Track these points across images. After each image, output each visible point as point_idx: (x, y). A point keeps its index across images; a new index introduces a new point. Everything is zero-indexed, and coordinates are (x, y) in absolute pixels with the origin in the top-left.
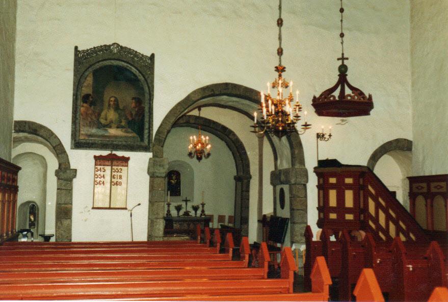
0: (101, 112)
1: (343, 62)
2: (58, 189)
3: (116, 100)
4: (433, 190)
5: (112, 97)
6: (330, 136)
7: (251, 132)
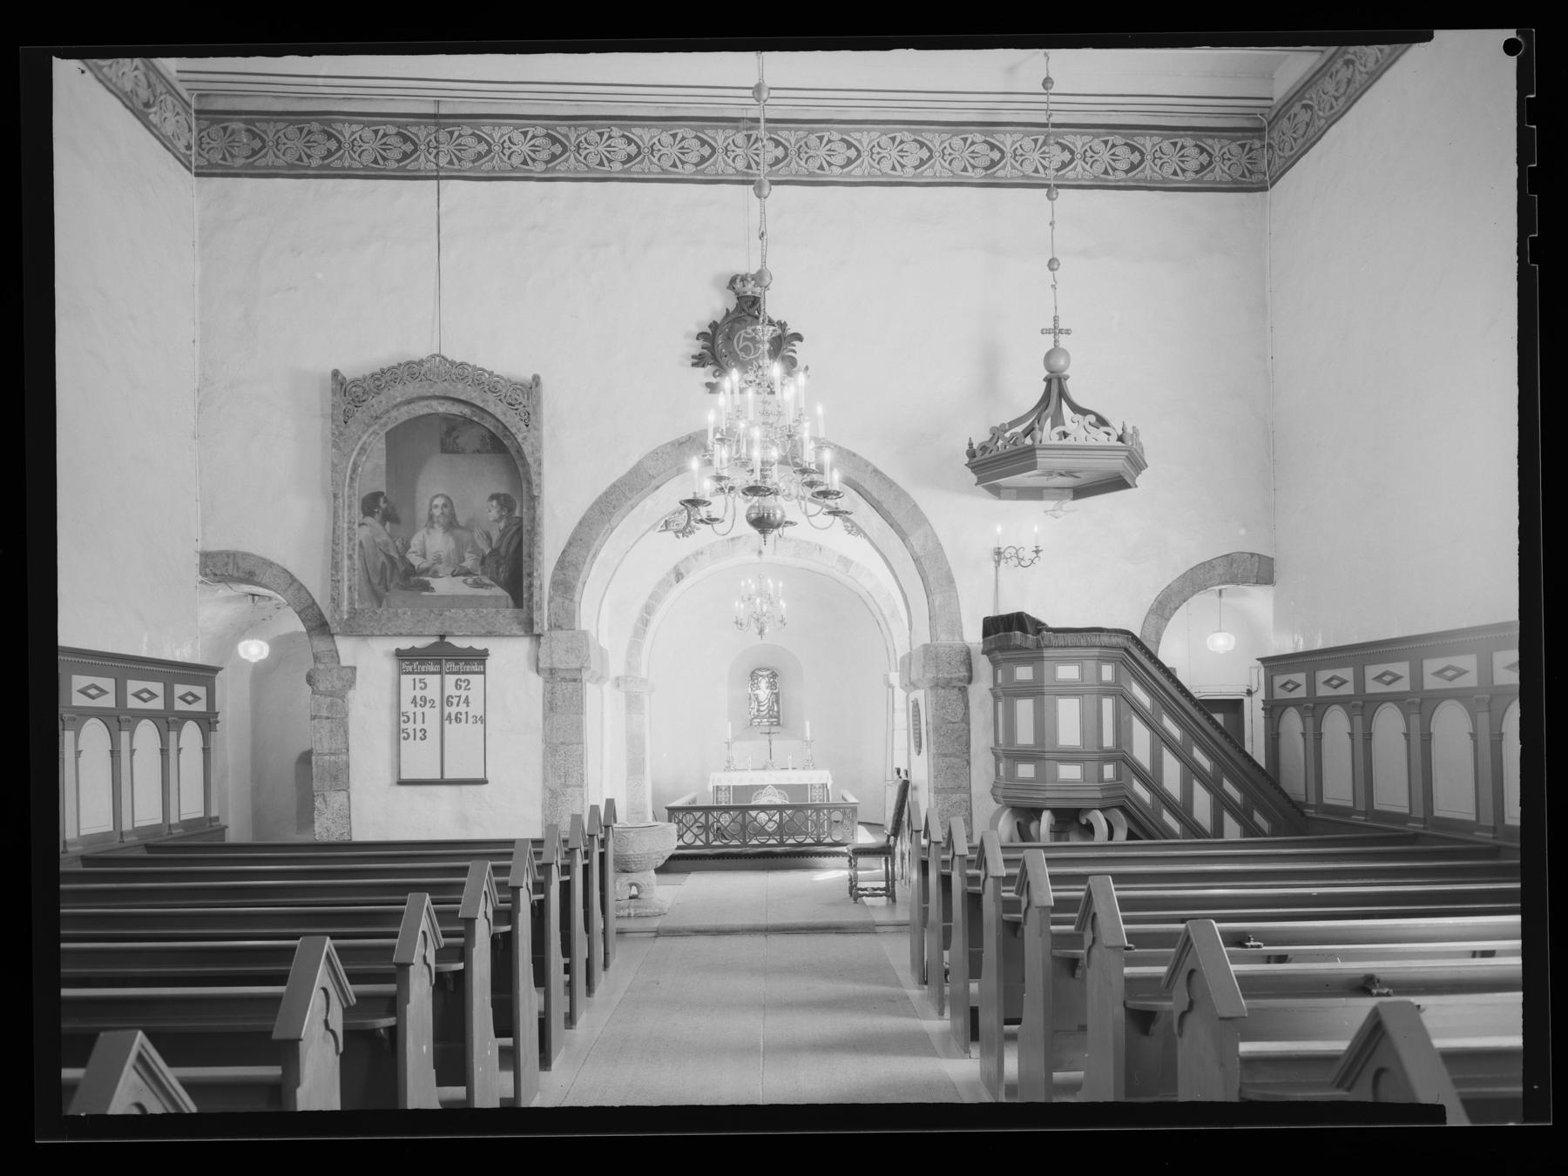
0: (411, 538)
3: (449, 503)
4: (1373, 688)
5: (437, 496)
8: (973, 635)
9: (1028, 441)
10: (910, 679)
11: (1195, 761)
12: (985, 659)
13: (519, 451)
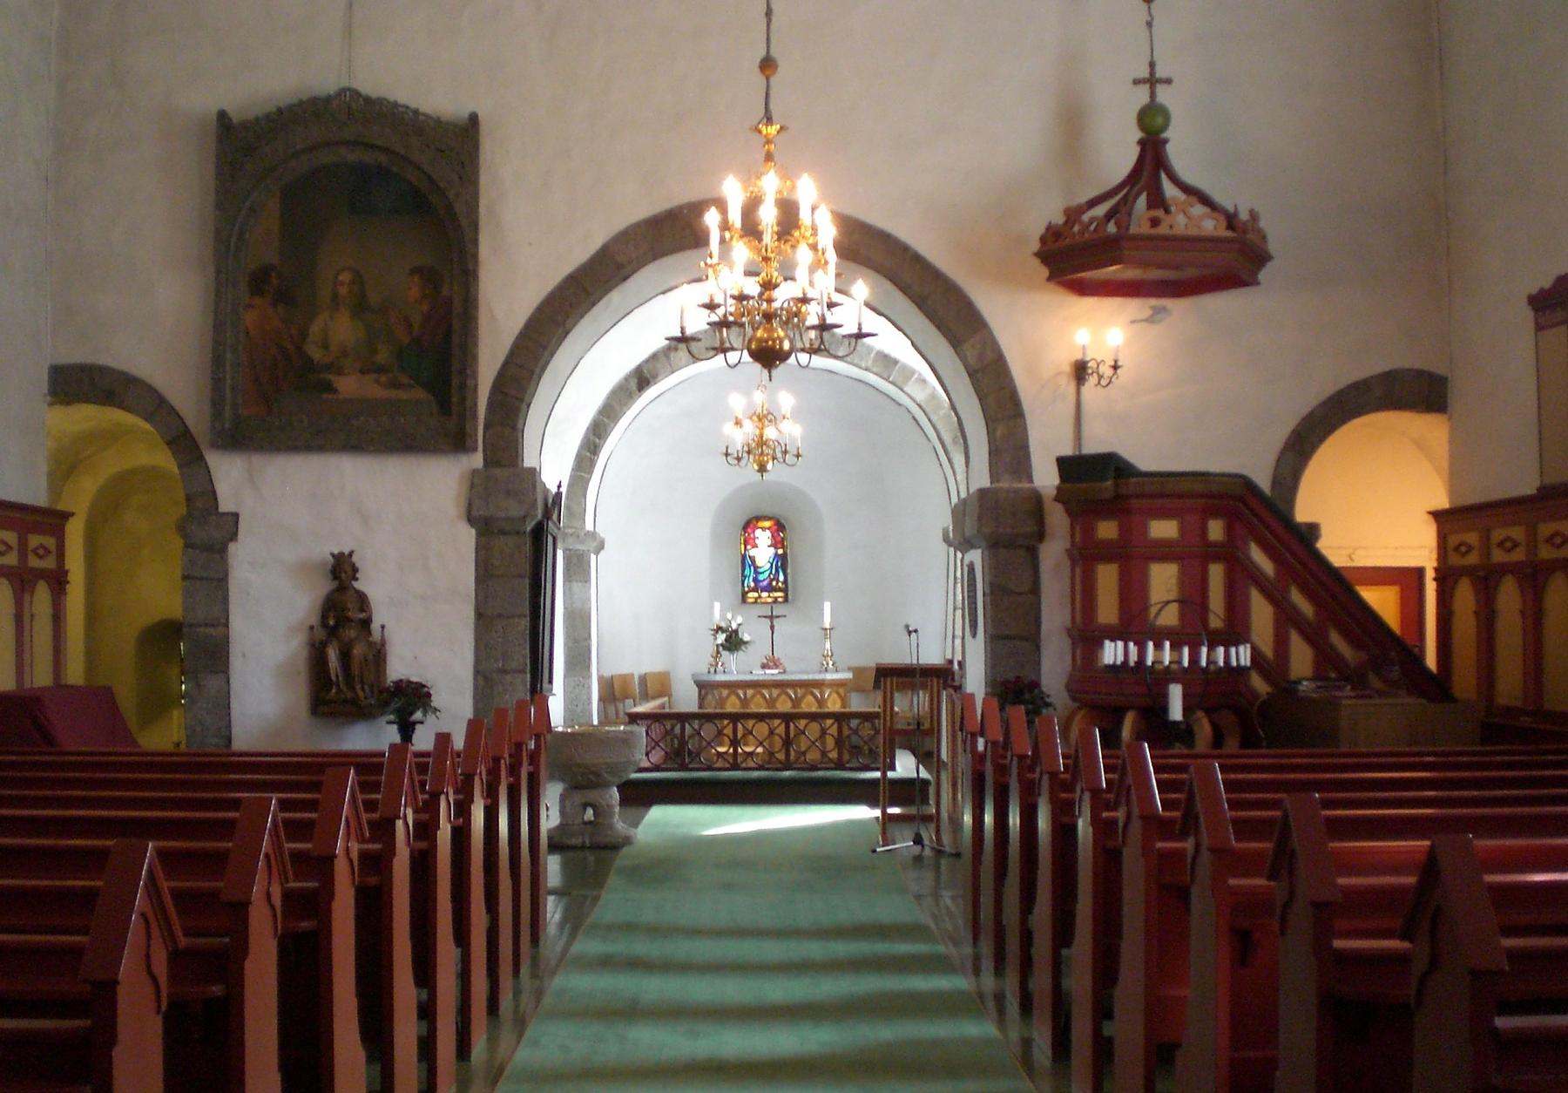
1: (1153, 95)
2: (185, 578)
6: (1115, 367)
8: (1046, 477)
9: (1111, 228)
10: (964, 534)
11: (1332, 647)
12: (1059, 508)
13: (450, 208)
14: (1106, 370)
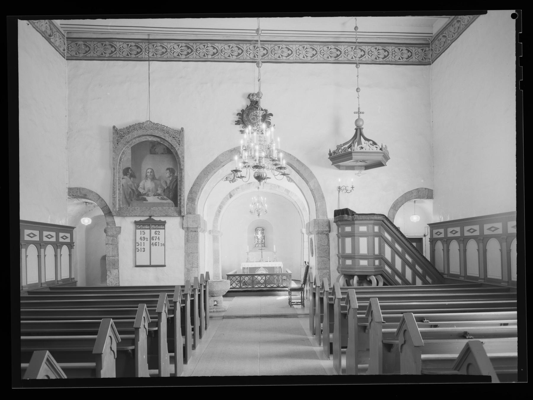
0: (140, 183)
3: (153, 171)
4: (467, 234)
5: (148, 169)
7: (308, 268)
8: (331, 216)
9: (350, 150)
10: (309, 231)
11: (406, 259)
12: (335, 224)
13: (177, 153)
14: (349, 188)
